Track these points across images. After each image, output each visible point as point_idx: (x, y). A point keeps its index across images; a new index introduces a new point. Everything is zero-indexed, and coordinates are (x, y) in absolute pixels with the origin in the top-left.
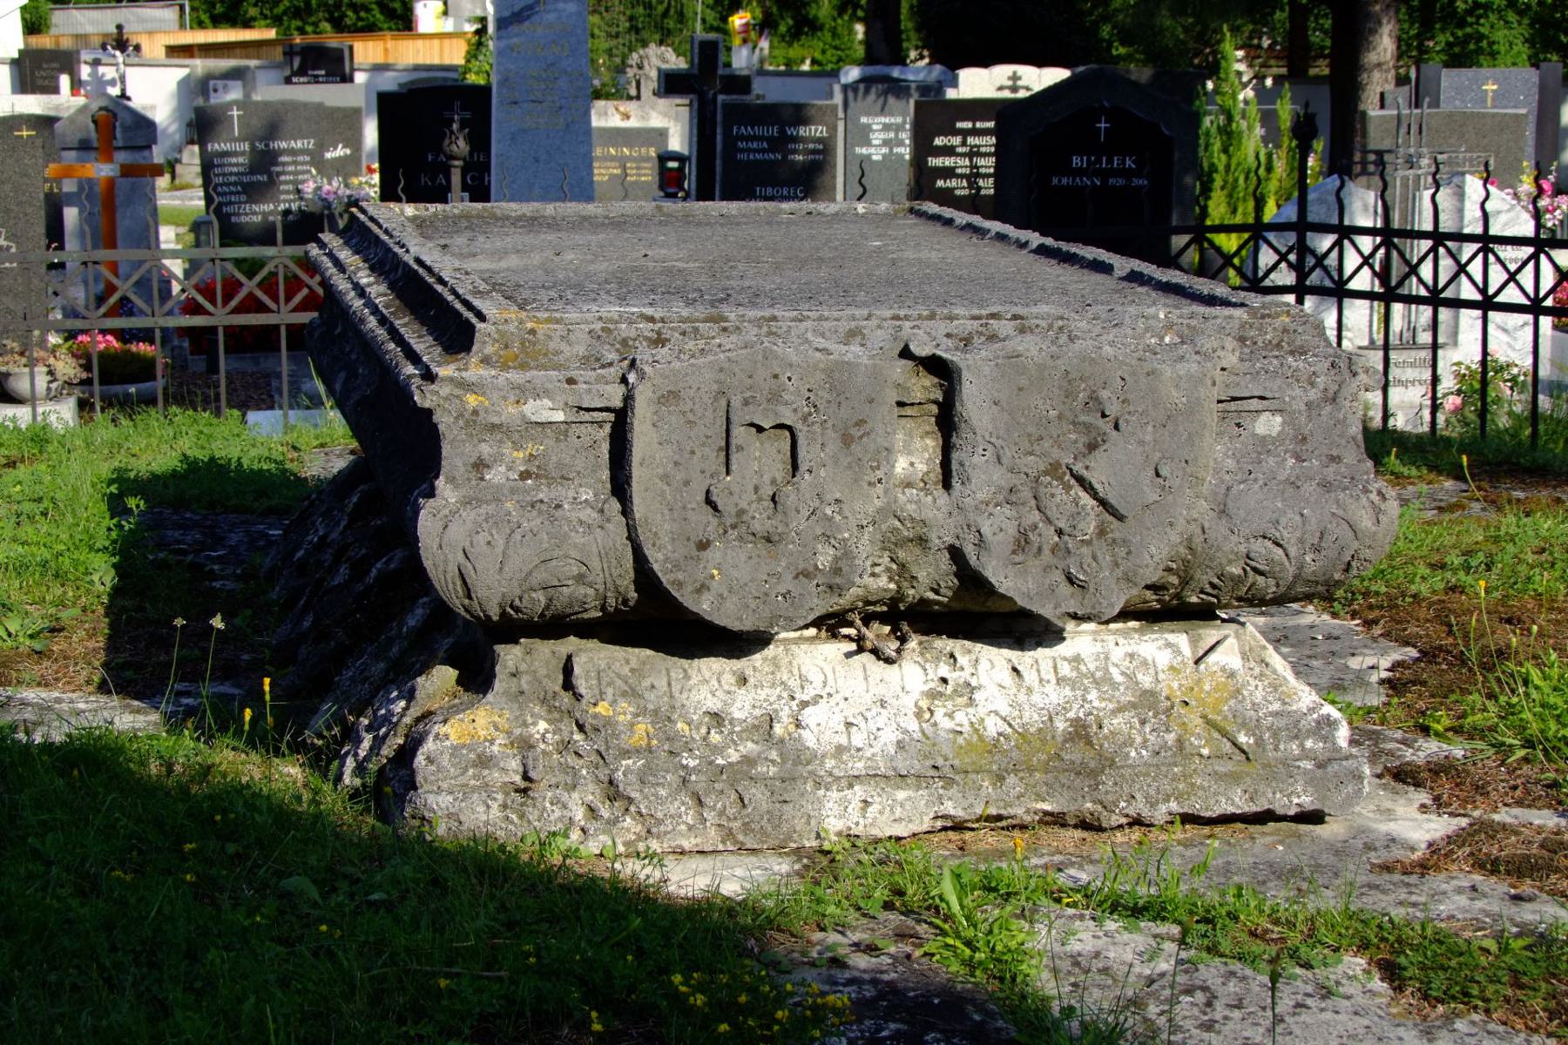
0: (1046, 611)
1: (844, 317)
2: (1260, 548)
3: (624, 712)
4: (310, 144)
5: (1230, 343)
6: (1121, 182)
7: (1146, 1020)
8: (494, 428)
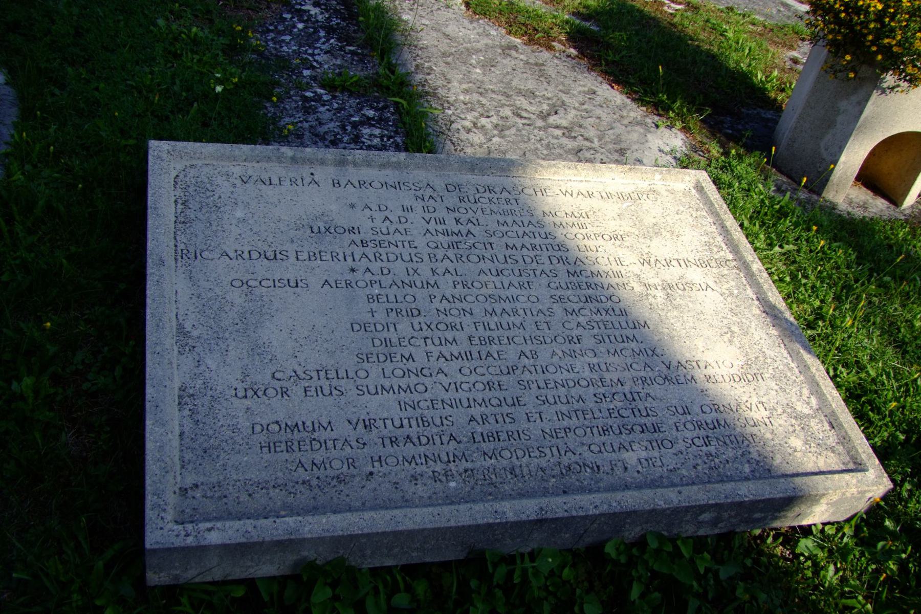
7: (394, 5)
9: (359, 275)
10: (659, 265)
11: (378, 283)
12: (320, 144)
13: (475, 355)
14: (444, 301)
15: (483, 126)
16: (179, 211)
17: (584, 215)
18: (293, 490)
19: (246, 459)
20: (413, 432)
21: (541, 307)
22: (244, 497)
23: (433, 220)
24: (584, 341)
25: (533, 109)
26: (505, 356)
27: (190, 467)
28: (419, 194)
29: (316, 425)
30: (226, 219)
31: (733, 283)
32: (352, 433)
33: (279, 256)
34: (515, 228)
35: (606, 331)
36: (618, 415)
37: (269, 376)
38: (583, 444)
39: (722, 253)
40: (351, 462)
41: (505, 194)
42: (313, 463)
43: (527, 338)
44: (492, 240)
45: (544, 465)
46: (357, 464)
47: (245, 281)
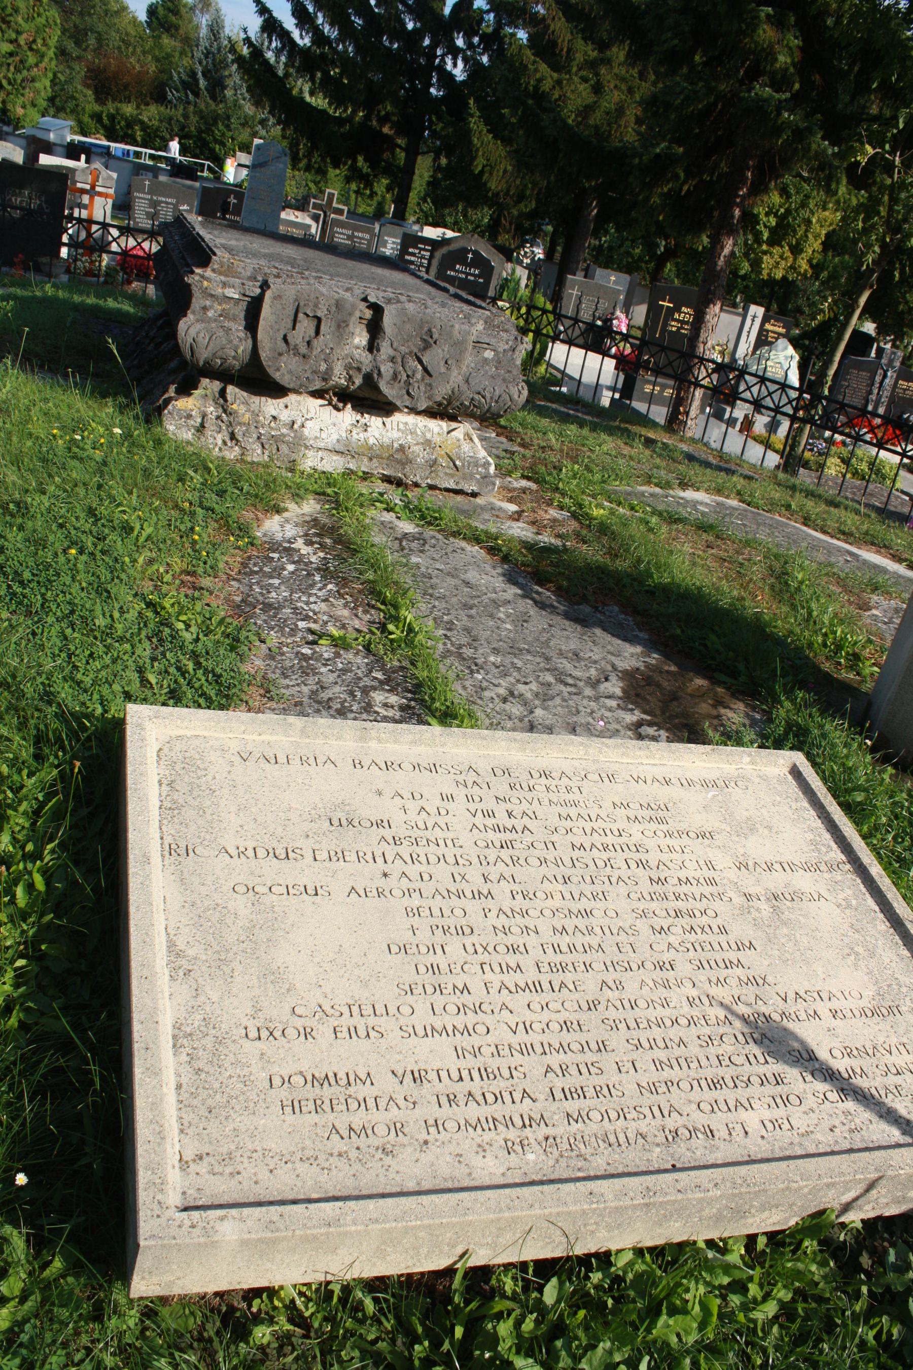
0: (398, 403)
1: (347, 283)
2: (477, 397)
3: (242, 409)
4: (174, 201)
5: (481, 322)
6: (472, 278)
8: (212, 296)
9: (392, 881)
10: (758, 869)
11: (418, 892)
12: (323, 712)
13: (546, 986)
14: (502, 916)
15: (521, 695)
16: (164, 794)
17: (663, 807)
18: (326, 1165)
19: (262, 1122)
20: (476, 1087)
21: (621, 924)
22: (263, 1174)
23: (479, 812)
24: (678, 966)
25: (577, 673)
26: (582, 988)
27: (191, 1131)
28: (460, 778)
29: (352, 1078)
30: (223, 805)
31: (850, 892)
32: (398, 1087)
33: (291, 855)
34: (581, 823)
35: (703, 954)
36: (729, 1063)
37: (288, 1010)
38: (690, 1101)
39: (832, 854)
40: (398, 1128)
41: (565, 780)
42: (351, 1129)
43: (609, 964)
44: (554, 838)
45: (644, 1130)
46: (405, 1130)
47: (250, 887)
